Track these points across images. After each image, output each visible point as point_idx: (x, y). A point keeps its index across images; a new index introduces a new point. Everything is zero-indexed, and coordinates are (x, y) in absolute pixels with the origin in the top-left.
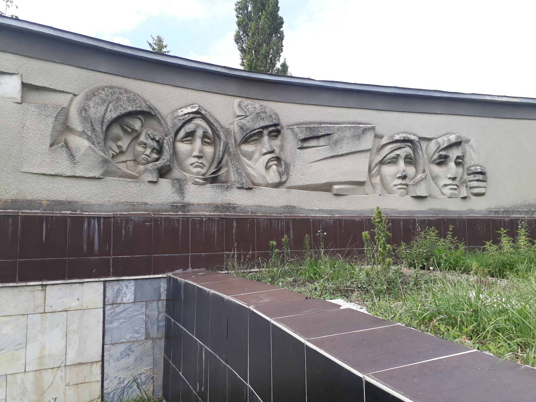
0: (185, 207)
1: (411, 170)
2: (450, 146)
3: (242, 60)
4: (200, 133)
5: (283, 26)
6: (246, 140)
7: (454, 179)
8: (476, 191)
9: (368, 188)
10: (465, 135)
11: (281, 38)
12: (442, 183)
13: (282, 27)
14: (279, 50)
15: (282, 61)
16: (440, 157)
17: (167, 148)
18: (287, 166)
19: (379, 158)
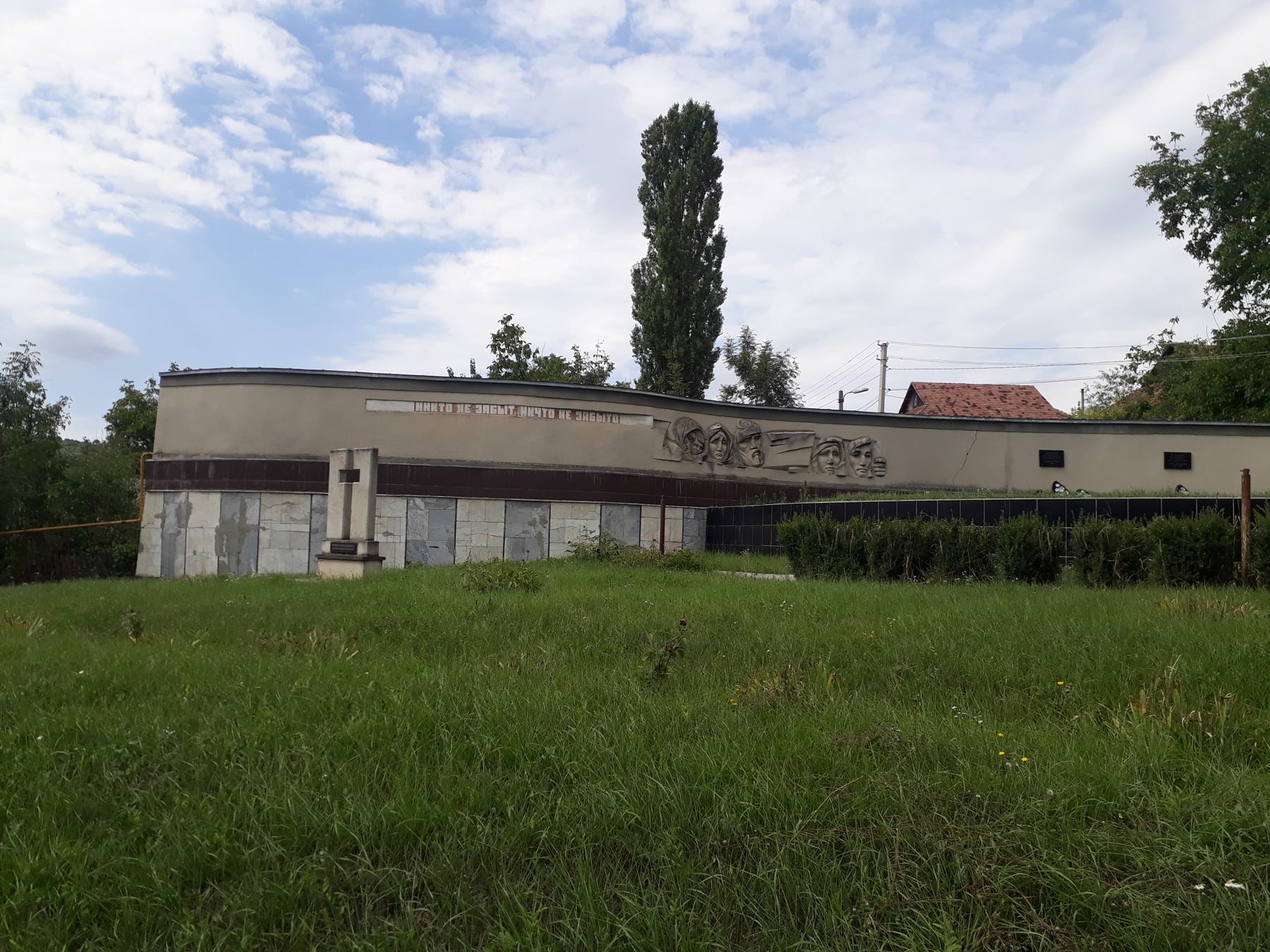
0: (713, 476)
1: (837, 459)
2: (863, 445)
3: (648, 227)
4: (721, 438)
5: (702, 104)
6: (742, 442)
7: (864, 466)
8: (878, 473)
9: (809, 469)
10: (873, 437)
11: (718, 194)
12: (856, 468)
13: (719, 176)
14: (712, 214)
15: (715, 232)
16: (856, 452)
17: (706, 446)
18: (764, 455)
19: (817, 452)
